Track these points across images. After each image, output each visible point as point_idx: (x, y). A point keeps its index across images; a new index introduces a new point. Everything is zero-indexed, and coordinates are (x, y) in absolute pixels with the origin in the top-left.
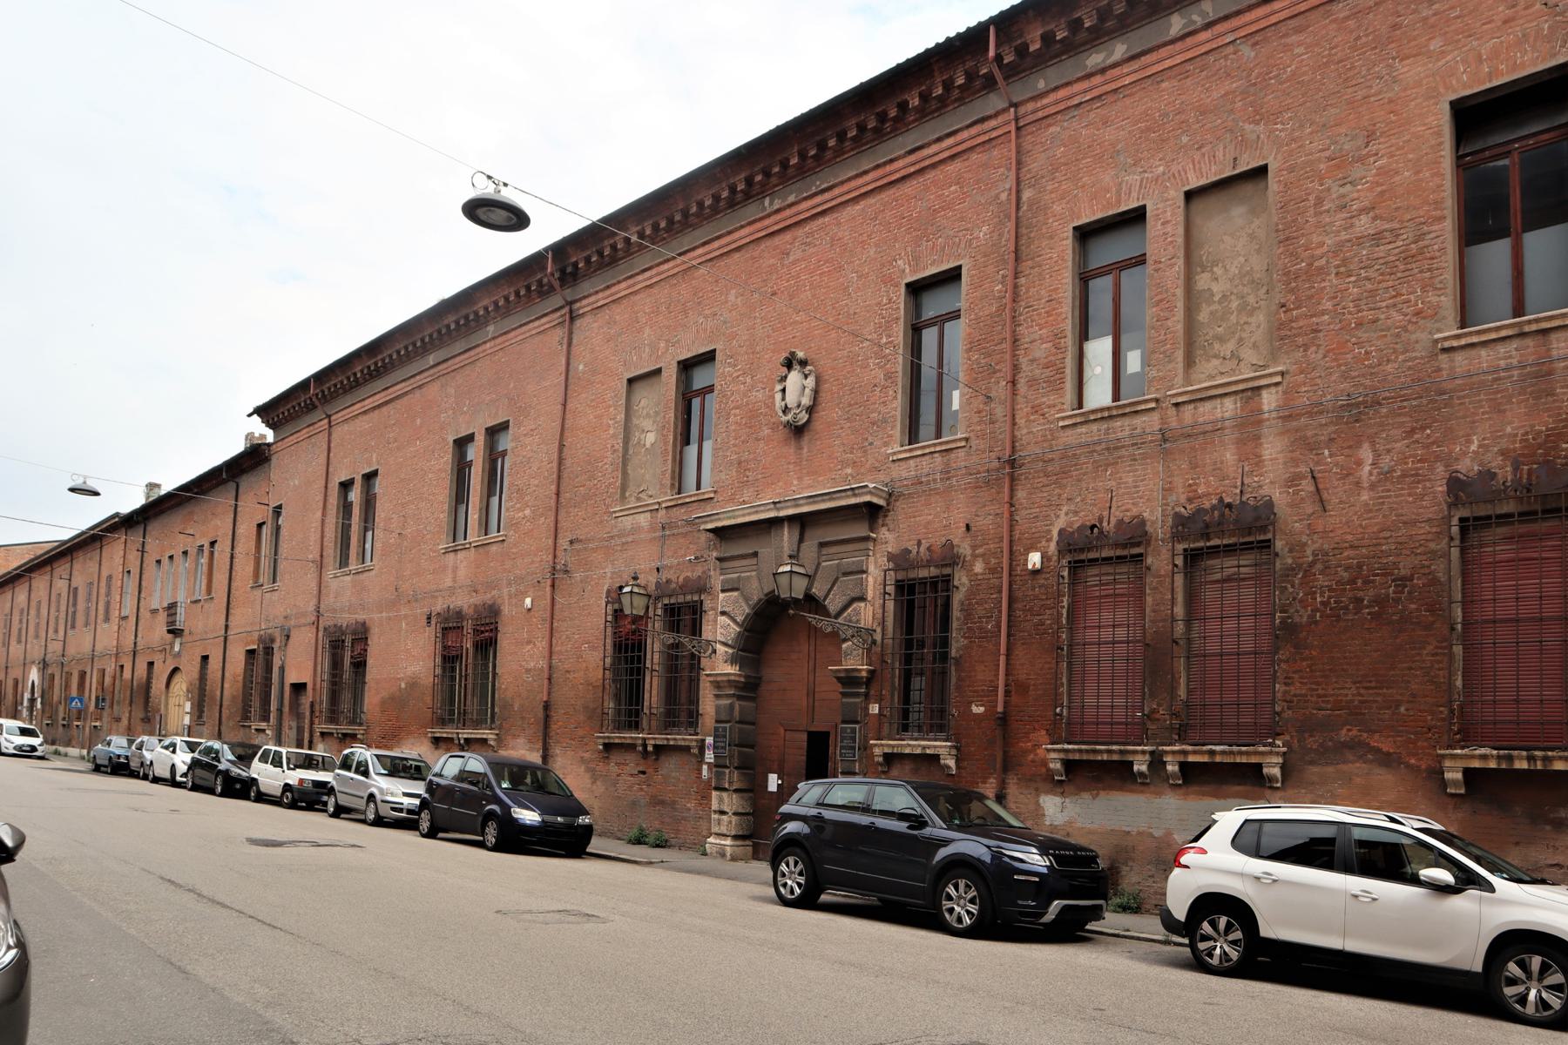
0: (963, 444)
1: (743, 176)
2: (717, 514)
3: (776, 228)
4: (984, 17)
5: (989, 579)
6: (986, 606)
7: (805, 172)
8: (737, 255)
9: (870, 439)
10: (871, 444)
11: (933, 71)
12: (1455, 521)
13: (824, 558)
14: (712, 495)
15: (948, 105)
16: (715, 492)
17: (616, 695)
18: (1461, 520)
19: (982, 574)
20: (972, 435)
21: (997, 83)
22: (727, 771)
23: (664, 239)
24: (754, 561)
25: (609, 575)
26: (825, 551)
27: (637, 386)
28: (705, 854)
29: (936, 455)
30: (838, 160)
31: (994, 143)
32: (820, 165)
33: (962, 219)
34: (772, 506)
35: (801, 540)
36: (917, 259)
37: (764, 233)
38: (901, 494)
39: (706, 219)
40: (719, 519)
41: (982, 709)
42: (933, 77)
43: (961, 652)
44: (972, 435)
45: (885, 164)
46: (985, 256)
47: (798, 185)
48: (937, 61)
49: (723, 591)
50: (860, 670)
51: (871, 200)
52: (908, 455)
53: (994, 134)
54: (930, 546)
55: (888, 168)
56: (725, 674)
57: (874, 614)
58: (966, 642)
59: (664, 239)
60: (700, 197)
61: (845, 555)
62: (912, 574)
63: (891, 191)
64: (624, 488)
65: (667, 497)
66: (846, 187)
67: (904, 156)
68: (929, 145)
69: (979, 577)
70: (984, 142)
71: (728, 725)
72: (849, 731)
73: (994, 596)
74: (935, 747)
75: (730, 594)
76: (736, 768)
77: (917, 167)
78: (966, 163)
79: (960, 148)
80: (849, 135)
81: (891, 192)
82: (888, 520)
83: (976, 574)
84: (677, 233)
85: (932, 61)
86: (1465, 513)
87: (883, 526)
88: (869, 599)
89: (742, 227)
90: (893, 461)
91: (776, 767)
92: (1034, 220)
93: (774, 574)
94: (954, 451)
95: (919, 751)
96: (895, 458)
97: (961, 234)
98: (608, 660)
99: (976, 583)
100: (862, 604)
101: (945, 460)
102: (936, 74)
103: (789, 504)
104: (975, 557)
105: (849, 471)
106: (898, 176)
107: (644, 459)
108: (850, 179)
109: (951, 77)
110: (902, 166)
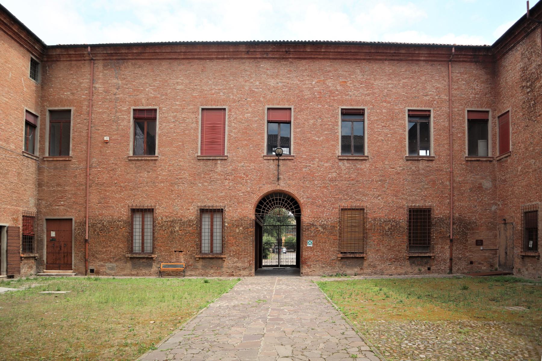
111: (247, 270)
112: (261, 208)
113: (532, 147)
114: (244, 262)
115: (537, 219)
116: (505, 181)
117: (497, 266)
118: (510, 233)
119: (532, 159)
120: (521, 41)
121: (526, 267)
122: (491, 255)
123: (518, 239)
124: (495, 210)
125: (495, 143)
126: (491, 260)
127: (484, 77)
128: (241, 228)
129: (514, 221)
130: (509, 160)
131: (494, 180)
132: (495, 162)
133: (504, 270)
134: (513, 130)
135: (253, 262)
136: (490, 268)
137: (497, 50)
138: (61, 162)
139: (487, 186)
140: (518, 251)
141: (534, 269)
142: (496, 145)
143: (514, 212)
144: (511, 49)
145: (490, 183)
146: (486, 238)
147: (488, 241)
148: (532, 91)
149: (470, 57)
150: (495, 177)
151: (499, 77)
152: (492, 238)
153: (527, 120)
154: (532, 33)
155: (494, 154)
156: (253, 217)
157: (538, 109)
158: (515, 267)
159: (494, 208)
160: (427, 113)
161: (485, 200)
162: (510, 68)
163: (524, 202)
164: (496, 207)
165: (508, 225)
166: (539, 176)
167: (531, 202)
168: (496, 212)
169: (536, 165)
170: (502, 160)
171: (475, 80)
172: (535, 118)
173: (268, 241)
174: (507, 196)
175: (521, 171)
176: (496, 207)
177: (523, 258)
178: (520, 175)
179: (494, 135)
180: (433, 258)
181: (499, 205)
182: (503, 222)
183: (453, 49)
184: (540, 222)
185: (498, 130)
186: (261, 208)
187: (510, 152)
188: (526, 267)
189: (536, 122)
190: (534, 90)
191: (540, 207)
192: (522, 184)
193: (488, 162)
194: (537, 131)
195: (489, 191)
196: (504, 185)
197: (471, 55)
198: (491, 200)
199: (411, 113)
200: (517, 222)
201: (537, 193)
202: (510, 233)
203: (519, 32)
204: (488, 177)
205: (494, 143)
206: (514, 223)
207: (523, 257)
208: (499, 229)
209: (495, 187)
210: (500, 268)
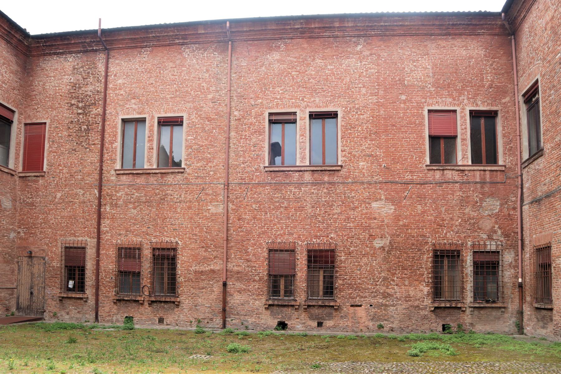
113: (80, 175)
115: (84, 258)
116: (32, 204)
117: (14, 310)
118: (39, 269)
119: (80, 189)
120: (74, 53)
121: (67, 311)
122: (7, 295)
123: (53, 277)
124: (14, 238)
125: (18, 155)
126: (7, 302)
127: (15, 67)
129: (48, 255)
130: (41, 181)
131: (14, 200)
132: (16, 178)
133: (26, 315)
134: (50, 147)
136: (6, 313)
137: (38, 45)
139: (6, 206)
140: (54, 291)
141: (79, 312)
142: (19, 158)
143: (47, 245)
144: (58, 54)
145: (10, 202)
146: (3, 273)
147: (4, 277)
148: (85, 114)
149: (3, 31)
150: (16, 197)
151: (32, 76)
152: (9, 273)
153: (75, 144)
155: (16, 167)
157: (92, 136)
158: (47, 311)
159: (12, 235)
161: (3, 224)
162: (52, 74)
163: (64, 235)
164: (15, 234)
165: (35, 261)
166: (88, 210)
167: (75, 236)
168: (14, 241)
169: (85, 196)
170: (30, 178)
171: (4, 64)
172: (87, 145)
174: (34, 224)
175: (60, 198)
176: (15, 234)
177: (60, 300)
178: (60, 204)
179: (18, 144)
180: (142, 302)
181: (19, 233)
182: (28, 255)
184: (88, 260)
185: (22, 139)
187: (45, 172)
188: (67, 311)
189: (88, 150)
190: (88, 115)
191: (89, 244)
192: (63, 214)
193: (10, 175)
194: (89, 160)
195: (8, 213)
196: (30, 209)
197: (5, 30)
198: (10, 225)
199: (274, 118)
200: (52, 257)
201: (85, 228)
202: (39, 269)
203: (76, 43)
204: (8, 195)
205: (17, 154)
206: (47, 258)
207: (62, 299)
208: (18, 262)
209: (15, 209)
210: (19, 312)
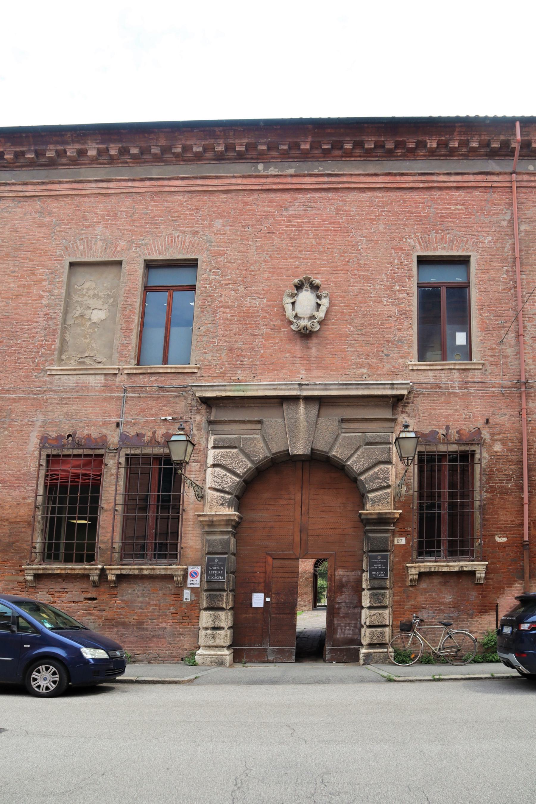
0: (481, 367)
1: (245, 141)
2: (225, 385)
3: (274, 187)
4: (518, 114)
5: (507, 456)
6: (506, 473)
7: (308, 158)
8: (223, 196)
9: (386, 352)
10: (387, 355)
11: (454, 131)
12: (44, 457)
13: (344, 430)
14: (196, 371)
15: (455, 156)
16: (199, 368)
17: (42, 530)
18: (48, 456)
19: (501, 452)
20: (487, 362)
21: (514, 156)
22: (225, 594)
23: (127, 163)
24: (258, 427)
25: (39, 424)
26: (345, 425)
27: (80, 270)
28: (195, 664)
29: (454, 371)
30: (343, 159)
31: (494, 190)
32: (324, 157)
33: (469, 228)
34: (297, 386)
35: (318, 416)
36: (101, 240)
37: (259, 187)
38: (422, 393)
39: (184, 161)
40: (225, 390)
41: (505, 539)
42: (453, 134)
43: (485, 502)
44: (487, 362)
45: (395, 175)
46: (490, 255)
47: (298, 164)
48: (461, 126)
49: (214, 448)
50: (394, 513)
51: (377, 194)
52: (428, 368)
53: (495, 185)
54: (460, 430)
55: (398, 178)
56: (226, 515)
57: (396, 474)
58: (488, 495)
59: (127, 163)
60: (188, 143)
61: (367, 430)
62: (433, 448)
63: (399, 194)
64: (62, 350)
65: (131, 366)
66: (353, 179)
67: (414, 175)
68: (438, 174)
69: (499, 454)
70: (486, 187)
71: (226, 556)
72: (379, 557)
73: (513, 467)
74: (472, 566)
75: (228, 450)
76: (230, 591)
77: (426, 185)
78: (469, 195)
79: (466, 184)
80: (366, 146)
81: (399, 194)
82: (409, 409)
83: (496, 452)
84: (145, 162)
85: (456, 125)
86: (49, 452)
87: (402, 412)
88: (394, 463)
89: (234, 177)
90: (413, 370)
91: (261, 587)
92: (531, 244)
93: (167, 442)
94: (471, 371)
95: (456, 569)
96: (415, 368)
97: (468, 236)
98: (40, 499)
99: (495, 460)
100: (390, 466)
101: (462, 375)
102: (456, 134)
103: (318, 387)
104: (494, 441)
105: (365, 371)
106: (407, 185)
107: (91, 331)
108: (359, 175)
109: (468, 140)
110: (410, 181)
111: (307, 606)
112: (317, 564)
114: (305, 601)
128: (304, 579)
135: (311, 601)
138: (422, 372)
154: (351, 663)
156: (312, 571)
160: (467, 259)
173: (322, 585)
183: (518, 124)
186: (317, 564)
